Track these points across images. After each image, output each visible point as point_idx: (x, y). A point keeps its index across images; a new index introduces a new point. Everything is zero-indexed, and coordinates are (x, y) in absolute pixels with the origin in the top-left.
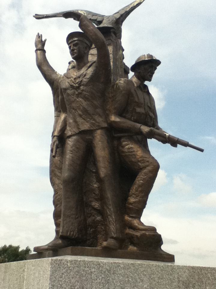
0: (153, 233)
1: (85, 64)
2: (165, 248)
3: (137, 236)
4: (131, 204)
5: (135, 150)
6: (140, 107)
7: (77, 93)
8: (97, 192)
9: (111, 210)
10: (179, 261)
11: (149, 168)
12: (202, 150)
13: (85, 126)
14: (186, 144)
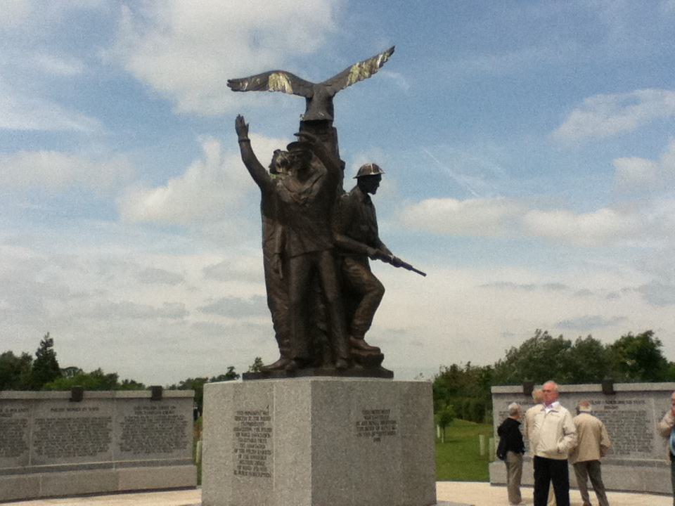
0: (377, 353)
1: (310, 176)
2: (385, 364)
3: (363, 357)
4: (357, 326)
5: (361, 272)
6: (363, 224)
7: (301, 210)
8: (323, 314)
9: (339, 332)
10: (396, 378)
11: (376, 292)
12: (424, 275)
13: (311, 247)
14: (409, 268)
